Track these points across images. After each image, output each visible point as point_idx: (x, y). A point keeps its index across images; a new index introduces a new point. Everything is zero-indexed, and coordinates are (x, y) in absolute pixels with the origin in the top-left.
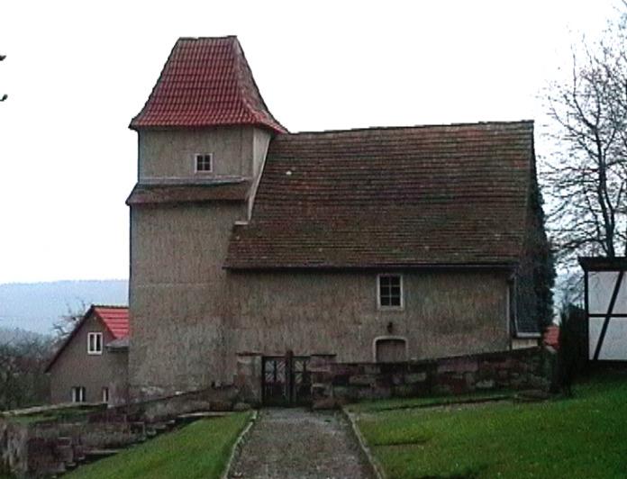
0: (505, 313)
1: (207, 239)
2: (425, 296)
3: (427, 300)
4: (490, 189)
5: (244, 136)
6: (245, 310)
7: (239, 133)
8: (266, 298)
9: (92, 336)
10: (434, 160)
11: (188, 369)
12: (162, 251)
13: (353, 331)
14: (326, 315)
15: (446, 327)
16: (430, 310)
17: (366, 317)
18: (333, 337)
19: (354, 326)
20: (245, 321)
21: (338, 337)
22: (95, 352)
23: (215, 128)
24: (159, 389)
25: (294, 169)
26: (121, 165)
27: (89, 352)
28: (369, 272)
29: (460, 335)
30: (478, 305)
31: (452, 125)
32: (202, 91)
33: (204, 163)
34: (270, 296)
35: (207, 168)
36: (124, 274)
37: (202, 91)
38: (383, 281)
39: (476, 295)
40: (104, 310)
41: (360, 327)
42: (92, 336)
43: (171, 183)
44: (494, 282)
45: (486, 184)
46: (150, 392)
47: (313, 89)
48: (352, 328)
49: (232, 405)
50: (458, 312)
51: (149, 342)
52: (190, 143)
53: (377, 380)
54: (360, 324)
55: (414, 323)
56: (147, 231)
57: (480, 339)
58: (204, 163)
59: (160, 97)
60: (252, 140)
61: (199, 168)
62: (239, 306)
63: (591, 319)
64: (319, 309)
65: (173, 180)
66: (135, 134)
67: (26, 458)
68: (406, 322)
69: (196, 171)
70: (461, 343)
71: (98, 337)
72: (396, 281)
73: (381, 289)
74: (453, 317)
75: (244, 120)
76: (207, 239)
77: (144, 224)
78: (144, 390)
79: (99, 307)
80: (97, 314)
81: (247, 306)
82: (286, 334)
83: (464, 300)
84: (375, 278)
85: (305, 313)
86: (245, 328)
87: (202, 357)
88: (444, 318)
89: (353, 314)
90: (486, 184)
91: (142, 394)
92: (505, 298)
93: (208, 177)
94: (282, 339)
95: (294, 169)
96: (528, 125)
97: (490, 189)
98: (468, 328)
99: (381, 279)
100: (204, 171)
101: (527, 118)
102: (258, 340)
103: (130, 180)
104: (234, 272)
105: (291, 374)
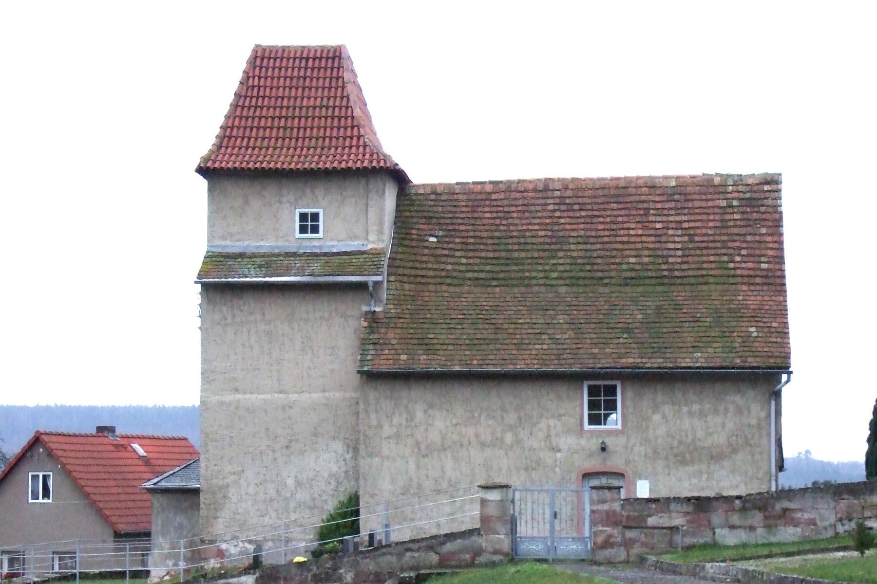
0: (769, 435)
2: (653, 413)
3: (657, 417)
4: (732, 265)
6: (387, 431)
8: (420, 415)
9: (35, 478)
11: (293, 516)
12: (252, 347)
13: (549, 462)
14: (509, 438)
15: (684, 455)
16: (662, 431)
17: (567, 442)
18: (518, 470)
19: (551, 454)
20: (387, 448)
21: (526, 469)
22: (41, 500)
27: (30, 501)
28: (574, 378)
29: (704, 467)
30: (730, 425)
31: (474, 183)
32: (291, 124)
33: (310, 224)
34: (425, 412)
35: (315, 229)
36: (862, 459)
37: (291, 124)
39: (726, 410)
40: (54, 439)
41: (559, 455)
42: (35, 478)
43: (262, 251)
44: (751, 393)
45: (725, 258)
46: (233, 550)
47: (443, 128)
48: (547, 457)
49: (473, 559)
50: (700, 434)
51: (233, 477)
52: (289, 194)
53: (688, 521)
54: (559, 451)
55: (636, 449)
56: (229, 321)
57: (733, 472)
58: (310, 224)
59: (238, 128)
60: (384, 192)
61: (303, 229)
64: (499, 429)
65: (314, 247)
66: (203, 183)
68: (626, 448)
70: (705, 477)
71: (45, 478)
72: (612, 391)
73: (590, 402)
74: (693, 440)
78: (224, 546)
79: (47, 434)
80: (44, 445)
82: (449, 465)
84: (583, 383)
85: (477, 436)
86: (388, 458)
87: (314, 499)
88: (680, 443)
89: (548, 436)
90: (725, 258)
91: (221, 554)
92: (769, 416)
93: (316, 243)
94: (444, 472)
96: (772, 182)
97: (732, 265)
98: (716, 457)
100: (309, 235)
102: (407, 473)
104: (372, 377)
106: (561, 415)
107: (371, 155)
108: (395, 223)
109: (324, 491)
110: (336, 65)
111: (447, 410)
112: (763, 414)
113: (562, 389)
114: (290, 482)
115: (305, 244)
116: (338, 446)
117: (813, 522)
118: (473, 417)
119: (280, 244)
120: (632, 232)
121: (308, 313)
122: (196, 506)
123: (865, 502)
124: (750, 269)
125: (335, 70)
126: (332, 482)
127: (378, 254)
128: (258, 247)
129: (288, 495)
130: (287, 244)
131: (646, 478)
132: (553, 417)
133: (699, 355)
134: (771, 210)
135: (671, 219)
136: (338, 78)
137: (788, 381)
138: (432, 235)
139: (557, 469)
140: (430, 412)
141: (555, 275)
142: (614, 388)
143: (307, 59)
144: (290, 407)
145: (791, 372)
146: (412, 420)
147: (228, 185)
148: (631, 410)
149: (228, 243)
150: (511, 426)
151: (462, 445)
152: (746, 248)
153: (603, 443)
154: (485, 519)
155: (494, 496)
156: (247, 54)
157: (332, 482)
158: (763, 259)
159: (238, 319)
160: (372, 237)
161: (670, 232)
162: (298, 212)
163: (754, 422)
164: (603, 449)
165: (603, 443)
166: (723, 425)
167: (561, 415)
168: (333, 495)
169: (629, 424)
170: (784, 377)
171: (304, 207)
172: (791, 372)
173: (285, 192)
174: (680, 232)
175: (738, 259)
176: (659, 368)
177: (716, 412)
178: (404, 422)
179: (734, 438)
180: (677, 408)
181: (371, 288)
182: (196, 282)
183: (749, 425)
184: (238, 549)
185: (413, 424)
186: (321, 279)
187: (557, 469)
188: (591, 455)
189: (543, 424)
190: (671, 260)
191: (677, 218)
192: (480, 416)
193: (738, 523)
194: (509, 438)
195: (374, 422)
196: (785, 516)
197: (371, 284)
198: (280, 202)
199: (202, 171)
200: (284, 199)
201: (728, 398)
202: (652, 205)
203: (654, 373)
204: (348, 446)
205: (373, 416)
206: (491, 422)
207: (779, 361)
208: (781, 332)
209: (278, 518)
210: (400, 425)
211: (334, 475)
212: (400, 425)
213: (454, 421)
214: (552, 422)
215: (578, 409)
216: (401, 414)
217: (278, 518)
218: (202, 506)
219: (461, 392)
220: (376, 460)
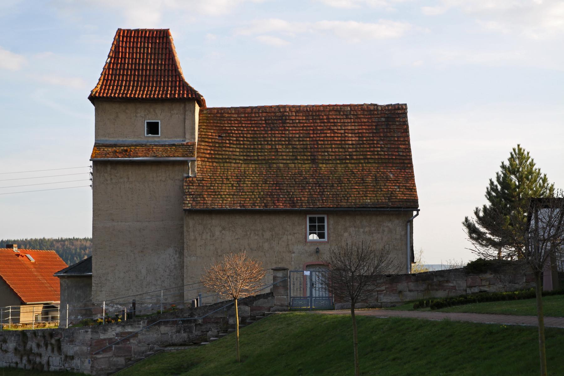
0: (407, 244)
1: (155, 192)
2: (344, 232)
3: (346, 234)
5: (187, 108)
7: (183, 105)
8: (217, 233)
14: (266, 246)
23: (163, 101)
24: (120, 307)
28: (302, 213)
32: (142, 70)
34: (221, 232)
37: (142, 70)
38: (311, 220)
41: (293, 255)
44: (396, 221)
47: (222, 77)
56: (109, 182)
58: (153, 128)
62: (195, 240)
65: (155, 141)
66: (92, 108)
67: (483, 257)
72: (322, 220)
75: (172, 96)
76: (155, 192)
77: (106, 175)
81: (202, 239)
83: (374, 235)
92: (406, 233)
99: (310, 218)
101: (383, 98)
106: (294, 234)
109: (163, 276)
110: (165, 41)
111: (233, 231)
112: (403, 233)
113: (296, 219)
114: (144, 272)
115: (150, 140)
116: (171, 251)
117: (454, 287)
118: (247, 235)
119: (136, 139)
121: (153, 178)
122: (90, 285)
125: (165, 44)
126: (167, 271)
128: (123, 141)
129: (142, 278)
130: (139, 139)
132: (290, 234)
136: (166, 49)
137: (417, 214)
139: (293, 263)
140: (223, 232)
142: (323, 218)
144: (144, 230)
145: (419, 210)
146: (213, 236)
147: (107, 106)
148: (332, 230)
149: (107, 139)
150: (267, 239)
153: (318, 248)
154: (275, 286)
155: (280, 274)
157: (167, 271)
159: (114, 181)
163: (398, 237)
165: (318, 248)
166: (382, 239)
167: (294, 234)
168: (168, 278)
169: (331, 238)
170: (415, 213)
171: (149, 119)
172: (419, 210)
173: (139, 111)
174: (353, 135)
176: (329, 208)
177: (378, 232)
178: (209, 237)
180: (357, 229)
182: (90, 160)
183: (396, 239)
184: (114, 309)
185: (214, 238)
186: (162, 159)
188: (311, 255)
189: (285, 238)
192: (250, 234)
193: (413, 288)
194: (266, 246)
195: (193, 238)
196: (440, 286)
198: (136, 116)
199: (92, 98)
200: (138, 115)
201: (384, 224)
204: (176, 251)
205: (192, 234)
206: (256, 237)
207: (412, 204)
208: (412, 189)
209: (137, 291)
210: (206, 239)
211: (168, 267)
212: (206, 239)
213: (236, 237)
214: (290, 237)
215: (304, 230)
216: (207, 233)
217: (137, 291)
218: (93, 284)
219: (240, 220)
220: (193, 258)
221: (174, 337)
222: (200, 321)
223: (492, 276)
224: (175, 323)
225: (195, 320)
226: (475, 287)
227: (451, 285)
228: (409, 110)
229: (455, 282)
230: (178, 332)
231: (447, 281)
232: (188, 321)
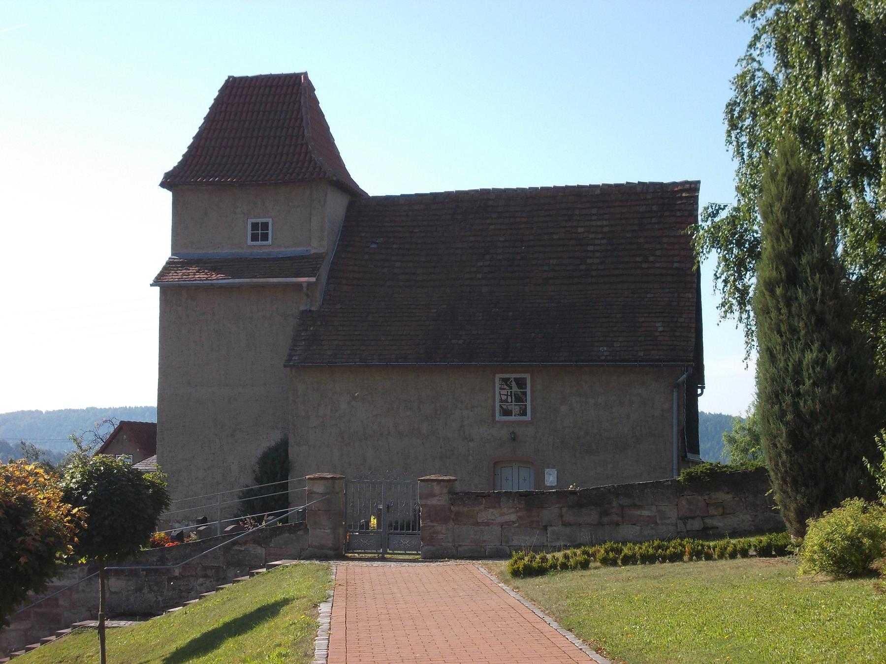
3: (564, 409)
10: (594, 211)
25: (379, 240)
26: (149, 232)
32: (261, 136)
33: (260, 232)
35: (265, 237)
36: (155, 404)
37: (261, 136)
41: (471, 444)
47: (399, 142)
54: (472, 440)
58: (260, 232)
61: (254, 238)
63: (107, 630)
69: (250, 242)
90: (639, 259)
92: (671, 407)
93: (266, 250)
95: (379, 240)
97: (645, 265)
100: (260, 243)
103: (161, 251)
105: (850, 274)
107: (314, 169)
108: (342, 231)
110: (295, 91)
115: (256, 250)
120: (555, 237)
123: (710, 498)
124: (663, 268)
127: (319, 257)
131: (554, 467)
133: (605, 349)
134: (686, 213)
135: (594, 223)
138: (373, 243)
140: (353, 403)
141: (479, 276)
143: (271, 87)
151: (382, 434)
152: (661, 249)
156: (219, 83)
158: (676, 259)
160: (315, 243)
161: (592, 236)
162: (250, 221)
164: (514, 439)
165: (513, 433)
174: (600, 236)
175: (651, 259)
179: (638, 428)
181: (305, 289)
187: (471, 458)
190: (589, 261)
191: (599, 223)
197: (305, 285)
202: (577, 212)
203: (212, 285)
206: (408, 413)
221: (132, 599)
222: (177, 573)
223: (730, 496)
224: (133, 574)
225: (168, 570)
226: (693, 518)
227: (646, 513)
228: (238, 74)
229: (654, 508)
230: (139, 590)
231: (635, 506)
232: (156, 571)
